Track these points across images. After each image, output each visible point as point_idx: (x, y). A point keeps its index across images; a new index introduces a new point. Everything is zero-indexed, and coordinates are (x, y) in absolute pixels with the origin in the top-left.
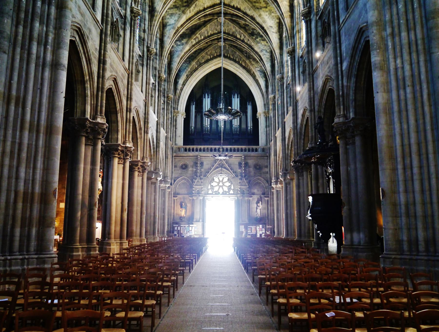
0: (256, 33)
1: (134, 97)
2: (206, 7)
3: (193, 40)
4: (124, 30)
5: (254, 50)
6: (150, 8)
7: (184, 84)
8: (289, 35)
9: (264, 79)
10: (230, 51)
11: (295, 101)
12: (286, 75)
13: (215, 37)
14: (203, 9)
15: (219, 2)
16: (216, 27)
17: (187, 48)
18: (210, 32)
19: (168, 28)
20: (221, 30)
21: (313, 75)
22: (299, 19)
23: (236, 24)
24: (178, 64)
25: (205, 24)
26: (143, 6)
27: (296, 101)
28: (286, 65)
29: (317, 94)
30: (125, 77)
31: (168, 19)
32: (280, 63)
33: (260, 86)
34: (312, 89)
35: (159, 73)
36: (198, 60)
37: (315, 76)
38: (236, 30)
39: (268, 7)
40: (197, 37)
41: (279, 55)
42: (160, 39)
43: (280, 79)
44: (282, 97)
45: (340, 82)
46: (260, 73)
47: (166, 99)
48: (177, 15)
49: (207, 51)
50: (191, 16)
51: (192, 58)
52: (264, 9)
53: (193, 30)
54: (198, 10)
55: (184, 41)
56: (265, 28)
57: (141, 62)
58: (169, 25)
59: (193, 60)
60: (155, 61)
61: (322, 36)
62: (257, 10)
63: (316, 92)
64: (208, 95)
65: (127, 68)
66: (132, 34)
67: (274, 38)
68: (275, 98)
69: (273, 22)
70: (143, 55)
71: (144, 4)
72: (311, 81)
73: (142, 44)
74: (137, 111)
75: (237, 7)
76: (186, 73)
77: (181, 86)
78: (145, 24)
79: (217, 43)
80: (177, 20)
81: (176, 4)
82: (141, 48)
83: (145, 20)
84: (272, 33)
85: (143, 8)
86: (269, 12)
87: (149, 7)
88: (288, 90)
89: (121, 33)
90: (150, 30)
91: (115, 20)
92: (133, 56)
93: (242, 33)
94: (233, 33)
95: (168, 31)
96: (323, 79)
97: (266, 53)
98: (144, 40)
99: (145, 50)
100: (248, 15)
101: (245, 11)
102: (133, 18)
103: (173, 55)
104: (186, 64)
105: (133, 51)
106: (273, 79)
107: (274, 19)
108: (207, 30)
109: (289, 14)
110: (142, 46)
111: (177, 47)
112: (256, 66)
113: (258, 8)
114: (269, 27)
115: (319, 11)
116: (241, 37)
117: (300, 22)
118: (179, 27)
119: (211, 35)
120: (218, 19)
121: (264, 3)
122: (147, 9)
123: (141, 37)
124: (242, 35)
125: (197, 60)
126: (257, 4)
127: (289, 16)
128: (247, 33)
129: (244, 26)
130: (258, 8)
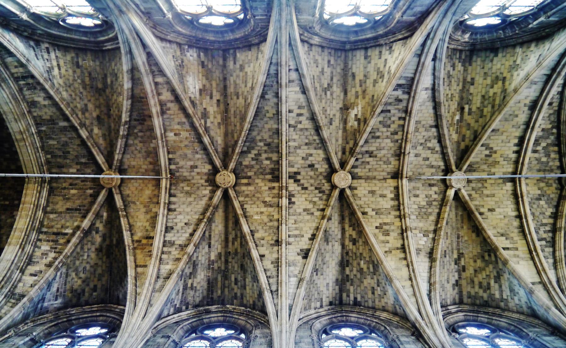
14: (518, 220)
31: (520, 300)
39: (504, 75)
48: (512, 279)
52: (507, 83)
54: (516, 231)
75: (516, 145)
81: (492, 276)
101: (523, 127)
113: (504, 97)
121: (495, 86)
126: (497, 102)
130: (504, 97)
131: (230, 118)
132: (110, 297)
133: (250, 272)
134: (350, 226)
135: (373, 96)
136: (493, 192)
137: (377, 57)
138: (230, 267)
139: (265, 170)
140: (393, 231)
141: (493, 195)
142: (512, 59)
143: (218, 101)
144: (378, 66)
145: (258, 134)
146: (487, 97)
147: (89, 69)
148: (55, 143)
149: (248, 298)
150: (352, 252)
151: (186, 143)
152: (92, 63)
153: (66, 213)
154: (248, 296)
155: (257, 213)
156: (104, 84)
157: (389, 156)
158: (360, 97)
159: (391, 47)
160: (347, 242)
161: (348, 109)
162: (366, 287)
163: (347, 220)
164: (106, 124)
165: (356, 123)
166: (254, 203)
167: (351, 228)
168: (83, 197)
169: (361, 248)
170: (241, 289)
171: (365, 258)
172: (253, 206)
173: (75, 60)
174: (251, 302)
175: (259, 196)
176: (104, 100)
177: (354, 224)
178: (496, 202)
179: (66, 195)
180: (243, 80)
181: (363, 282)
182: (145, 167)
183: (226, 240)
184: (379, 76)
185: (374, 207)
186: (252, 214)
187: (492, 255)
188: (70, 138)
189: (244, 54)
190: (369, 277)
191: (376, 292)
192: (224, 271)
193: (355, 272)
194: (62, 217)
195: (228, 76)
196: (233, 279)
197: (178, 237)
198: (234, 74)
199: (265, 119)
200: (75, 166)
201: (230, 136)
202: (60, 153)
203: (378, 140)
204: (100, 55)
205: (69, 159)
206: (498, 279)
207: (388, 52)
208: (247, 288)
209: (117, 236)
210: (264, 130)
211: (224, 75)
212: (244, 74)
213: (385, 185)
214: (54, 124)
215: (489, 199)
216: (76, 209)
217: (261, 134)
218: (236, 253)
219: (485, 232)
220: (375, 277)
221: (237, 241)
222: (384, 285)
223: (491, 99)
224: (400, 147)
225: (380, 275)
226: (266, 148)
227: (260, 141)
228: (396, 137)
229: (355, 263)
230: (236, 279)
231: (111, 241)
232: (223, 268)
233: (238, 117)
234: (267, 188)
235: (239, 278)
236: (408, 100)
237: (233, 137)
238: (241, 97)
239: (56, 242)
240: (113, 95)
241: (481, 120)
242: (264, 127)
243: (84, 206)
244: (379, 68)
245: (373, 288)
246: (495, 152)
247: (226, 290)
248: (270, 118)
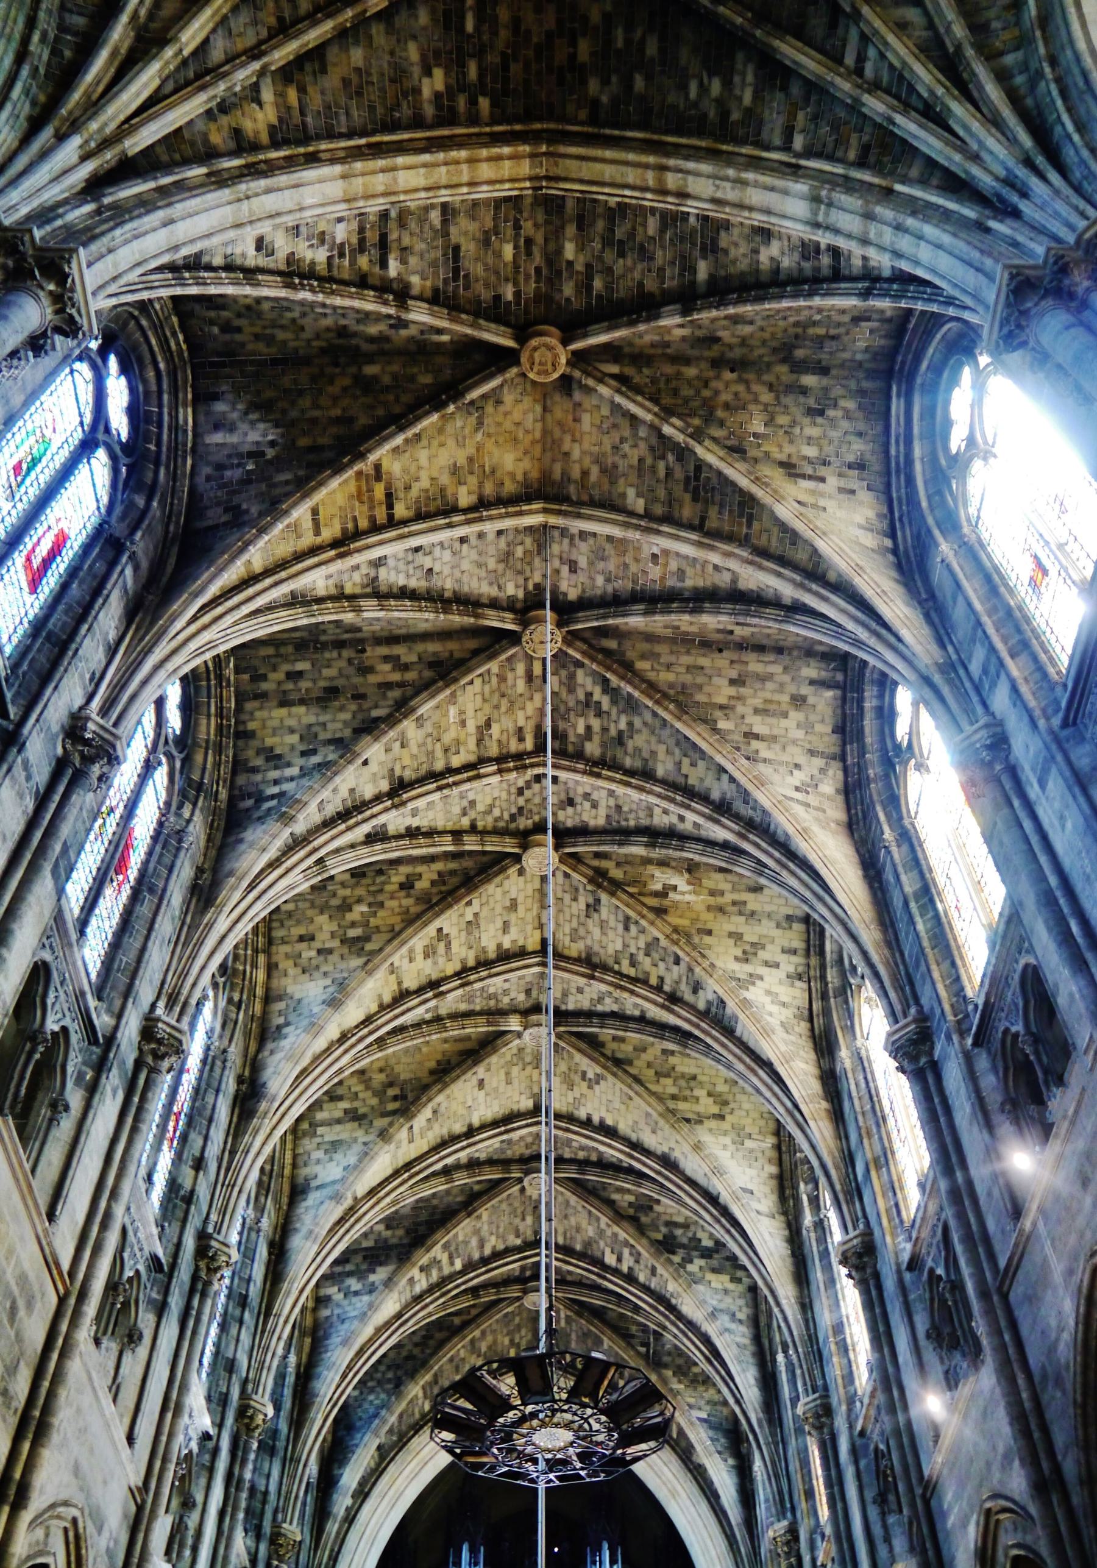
0: (685, 1241)
1: (63, 1419)
2: (476, 1123)
3: (415, 1272)
4: (92, 1089)
5: (680, 1316)
6: (244, 1087)
7: (362, 1493)
8: (838, 1187)
9: (731, 1461)
10: (573, 1336)
11: (919, 1491)
12: (841, 1390)
13: (512, 1267)
15: (529, 1104)
16: (517, 1221)
17: (390, 1306)
18: (493, 1243)
19: (313, 1198)
20: (537, 1233)
21: (1005, 1297)
22: (870, 1115)
23: (597, 1202)
24: (344, 1376)
25: (471, 1201)
26: (211, 1070)
27: (926, 1488)
28: (833, 1347)
29: (1059, 1382)
30: (38, 1305)
31: (318, 1161)
32: (804, 1345)
33: (717, 1496)
34: (1016, 1367)
35: (243, 1391)
36: (436, 1376)
37: (1017, 1293)
38: (601, 1233)
40: (436, 1262)
41: (796, 1307)
42: (271, 1245)
43: (817, 1416)
44: (839, 1506)
46: (711, 1433)
47: (263, 1548)
49: (477, 1333)
50: (413, 1155)
51: (410, 1365)
52: (713, 1124)
53: (422, 1230)
54: (445, 1131)
55: (380, 1275)
56: (725, 1198)
57: (154, 1295)
58: (318, 1188)
59: (412, 1375)
60: (234, 1331)
61: (1008, 1107)
62: (685, 1127)
63: (1044, 1376)
64: (473, 1552)
65: (66, 1266)
66: (129, 1120)
67: (767, 1237)
68: (796, 1539)
69: (753, 1172)
70: (173, 1266)
71: (218, 1063)
72: (1003, 1323)
73: (180, 1214)
74: (77, 1537)
75: (602, 1122)
76: (377, 1436)
77: (349, 1501)
78: (206, 1138)
79: (518, 1299)
80: (356, 1167)
81: (356, 1104)
82: (172, 1230)
83: (210, 1120)
84: (753, 1214)
85: (210, 1076)
86: (733, 1135)
87: (240, 1080)
88: (863, 1463)
89: (75, 1098)
90: (228, 1170)
91: (129, 1273)
92: (108, 1215)
93: (626, 1244)
94: (588, 1244)
95: (312, 1212)
96: (1076, 1279)
97: (733, 1326)
98: (189, 1199)
99: (189, 1243)
100: (647, 1152)
101: (634, 1137)
102: (149, 1060)
103: (327, 1336)
104: (383, 1396)
105: (114, 1195)
106: (776, 1444)
107: (758, 1164)
108: (477, 1232)
109: (825, 1105)
110: (176, 1226)
111: (345, 1302)
112: (692, 1401)
113: (688, 1121)
114: (740, 1193)
115: (967, 1016)
116: (619, 1260)
117: (878, 1125)
118: (359, 1195)
119: (496, 1255)
120: (526, 1183)
122: (230, 1085)
123: (180, 1186)
124: (626, 1252)
125: (428, 1377)
126: (682, 1106)
127: (823, 1114)
128: (644, 1241)
129: (631, 1211)
130: (688, 1121)
131: (688, 652)
132: (213, 364)
133: (322, 719)
134: (440, 874)
135: (709, 933)
136: (516, 1082)
137: (786, 945)
138: (327, 655)
139: (563, 718)
140: (435, 963)
141: (509, 1082)
142: (754, 1130)
143: (731, 632)
144: (769, 947)
145: (645, 724)
146: (693, 1084)
147: (846, 339)
148: (651, 232)
149: (258, 714)
150: (384, 883)
151: (633, 568)
152: (861, 344)
153: (446, 248)
154: (264, 714)
155: (462, 712)
156: (804, 361)
157: (589, 942)
158: (711, 900)
159: (800, 977)
160: (404, 870)
161: (689, 871)
162: (312, 921)
163: (452, 865)
164: (695, 353)
165: (658, 887)
166: (485, 700)
167: (435, 877)
168: (493, 278)
169: (394, 904)
170: (277, 691)
171: (375, 914)
172: (479, 698)
173: (875, 316)
174: (251, 726)
175: (503, 709)
176: (761, 357)
177: (444, 883)
178: (496, 1089)
179: (496, 234)
180: (770, 701)
181: (322, 913)
182: (576, 454)
183: (393, 639)
184: (748, 948)
185: (482, 915)
186: (460, 699)
187: (396, 1105)
188: (661, 270)
189: (829, 712)
190: (334, 926)
191: (304, 945)
192: (317, 641)
193: (343, 892)
194: (433, 239)
195: (785, 659)
196: (300, 666)
197: (396, 568)
198: (786, 678)
199: (677, 751)
200: (582, 259)
201: (645, 646)
202: (619, 233)
203: (620, 927)
204: (883, 366)
205: (603, 251)
206: (354, 1116)
207: (791, 969)
208: (283, 711)
209: (387, 380)
210: (653, 739)
211: (790, 650)
212: (784, 707)
213: (529, 928)
214: (704, 249)
215: (503, 1076)
216: (456, 271)
217: (645, 731)
218: (365, 670)
219: (440, 1091)
220: (336, 943)
221: (394, 670)
222: (324, 969)
223: (687, 1093)
224: (605, 968)
225: (342, 957)
226: (613, 732)
227: (630, 724)
228: (625, 963)
229: (360, 891)
230: (300, 674)
231: (370, 359)
232: (323, 638)
233: (688, 678)
234: (521, 722)
235: (304, 684)
236: (692, 1008)
237: (643, 657)
238: (732, 691)
239: (361, 247)
240: (771, 387)
241: (651, 1072)
242: (660, 742)
243: (467, 287)
244: (763, 947)
245: (312, 938)
246: (590, 1087)
247: (270, 651)
248: (679, 764)
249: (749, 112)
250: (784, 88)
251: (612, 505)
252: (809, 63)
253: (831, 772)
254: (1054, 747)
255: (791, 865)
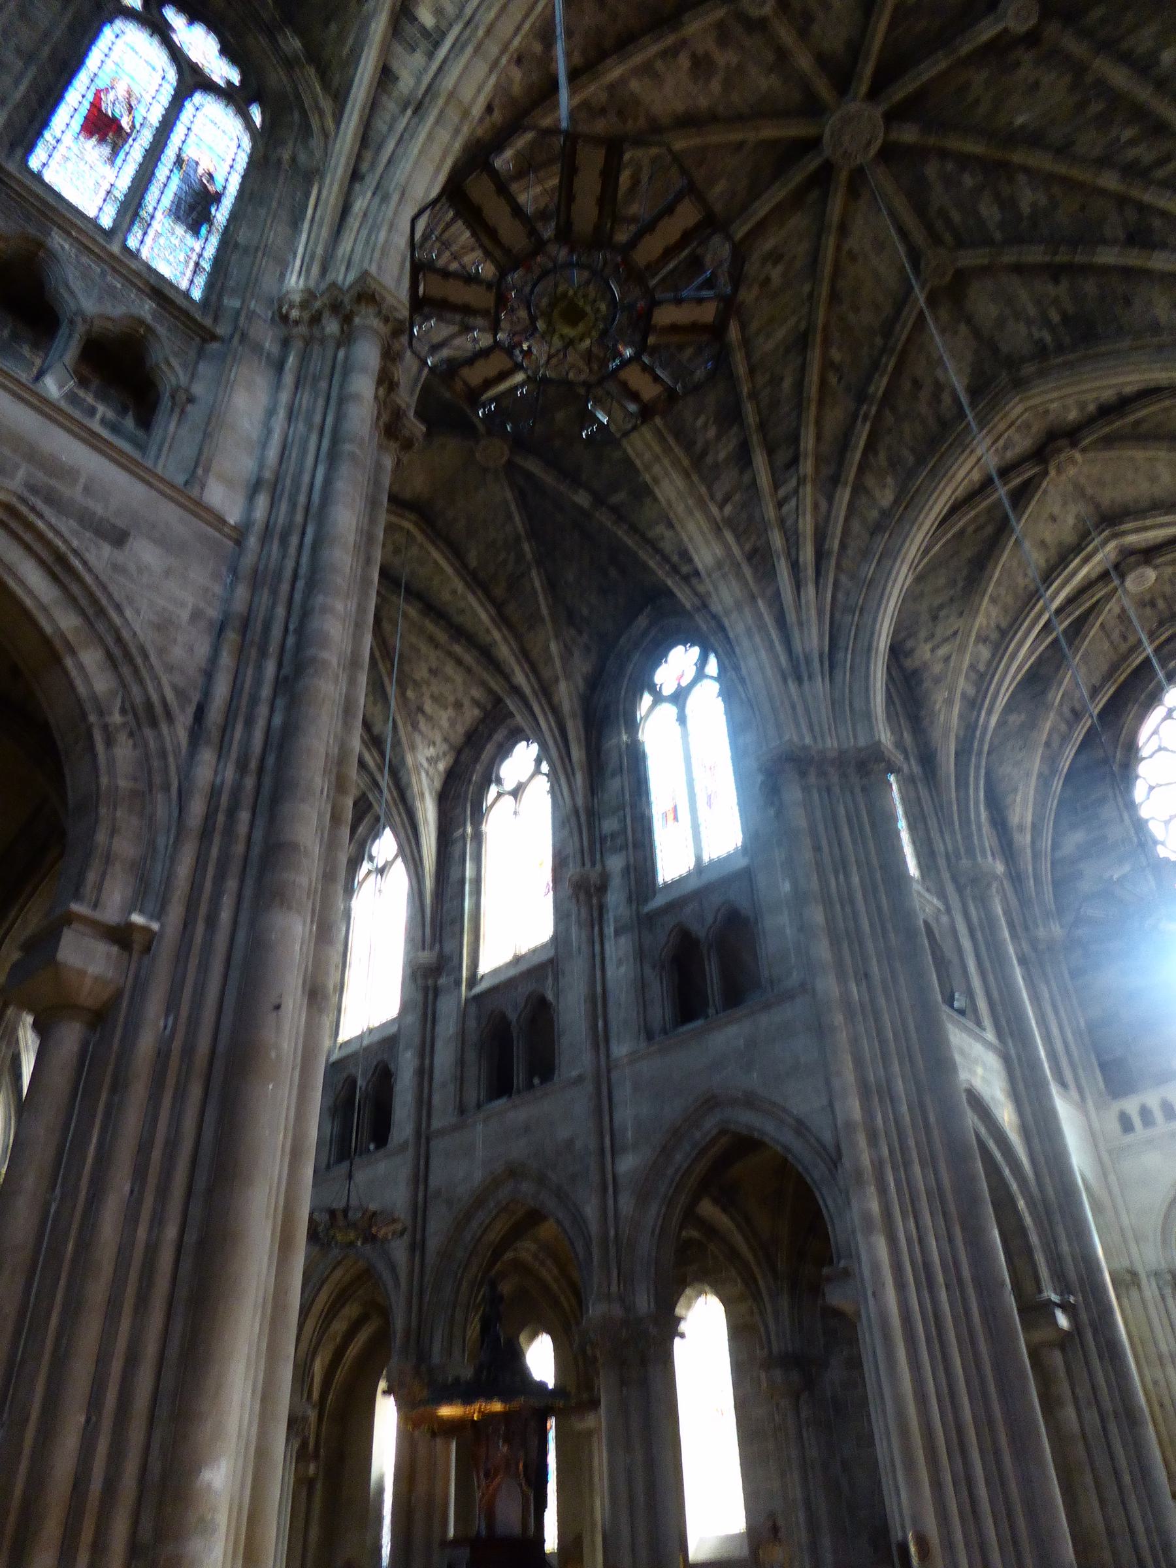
45: (611, 1202)
249: (716, 465)
250: (742, 472)
251: (456, 553)
252: (764, 480)
253: (448, 757)
254: (238, 358)
255: (401, 807)
